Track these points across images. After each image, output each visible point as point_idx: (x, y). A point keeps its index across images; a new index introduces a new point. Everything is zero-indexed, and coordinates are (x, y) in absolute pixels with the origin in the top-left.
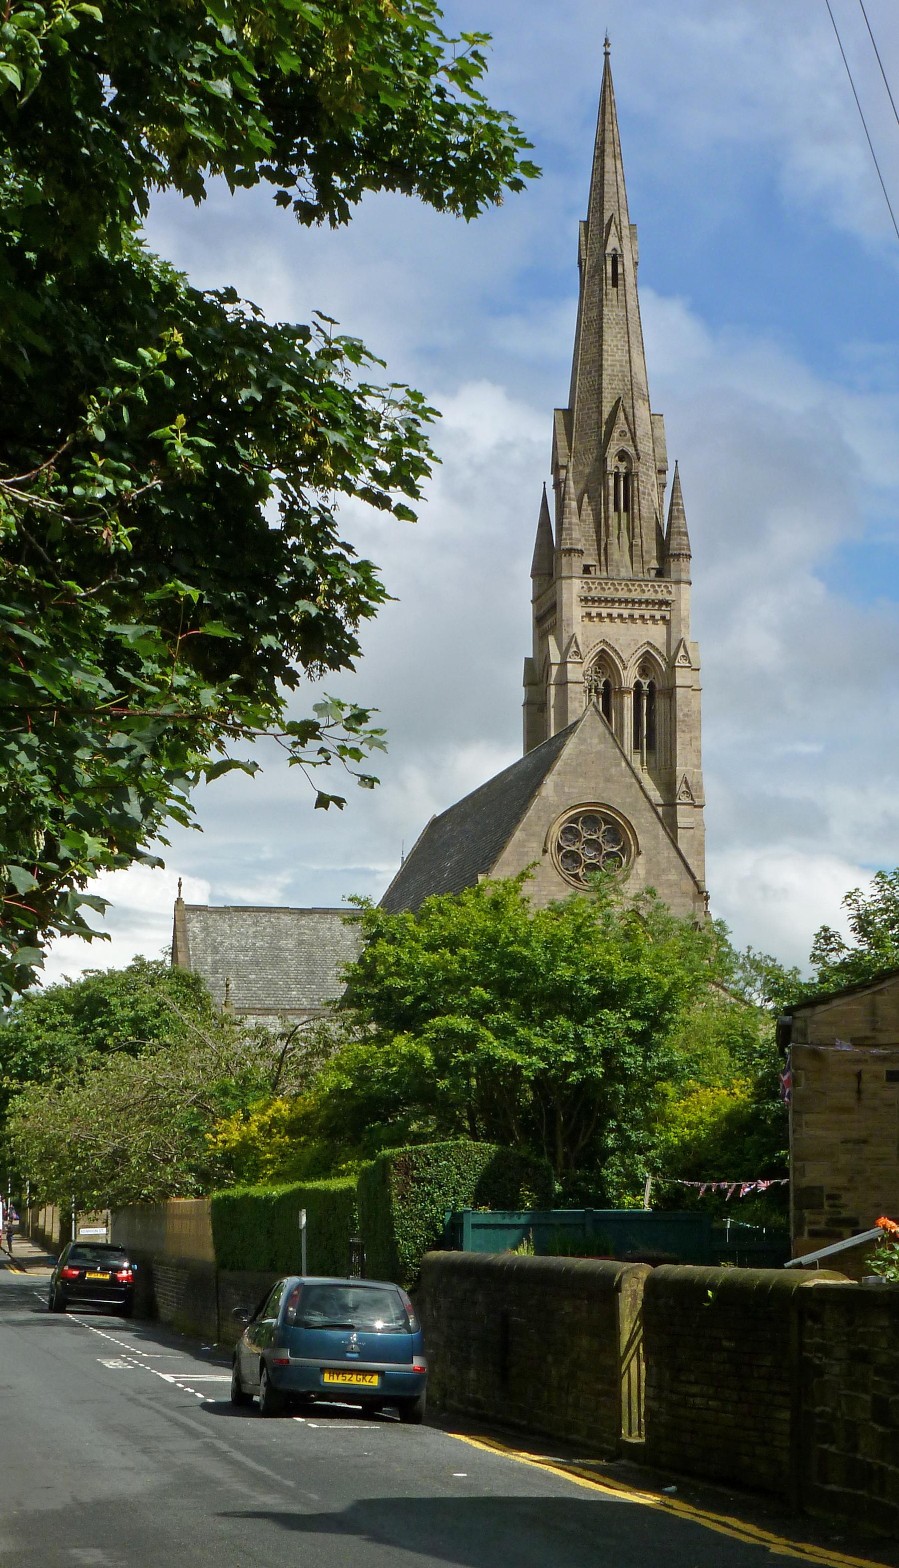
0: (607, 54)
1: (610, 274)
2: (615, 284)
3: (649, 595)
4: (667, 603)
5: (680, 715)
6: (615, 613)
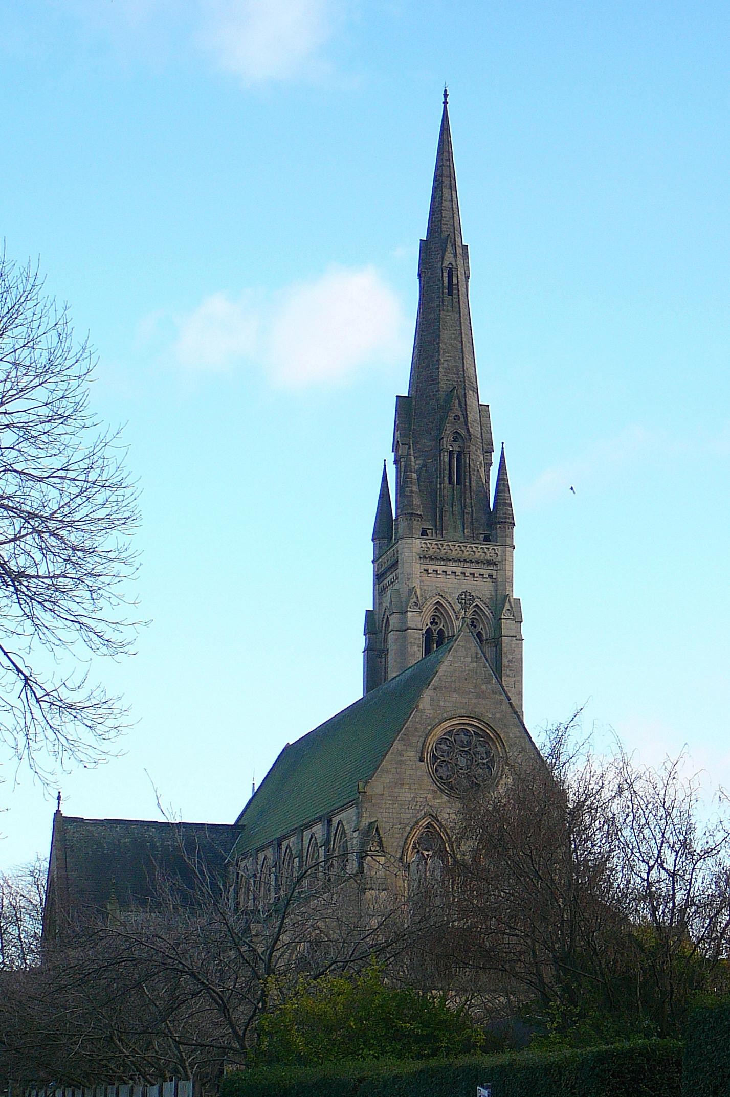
0: (445, 103)
1: (446, 284)
2: (450, 293)
4: (490, 563)
5: (505, 661)
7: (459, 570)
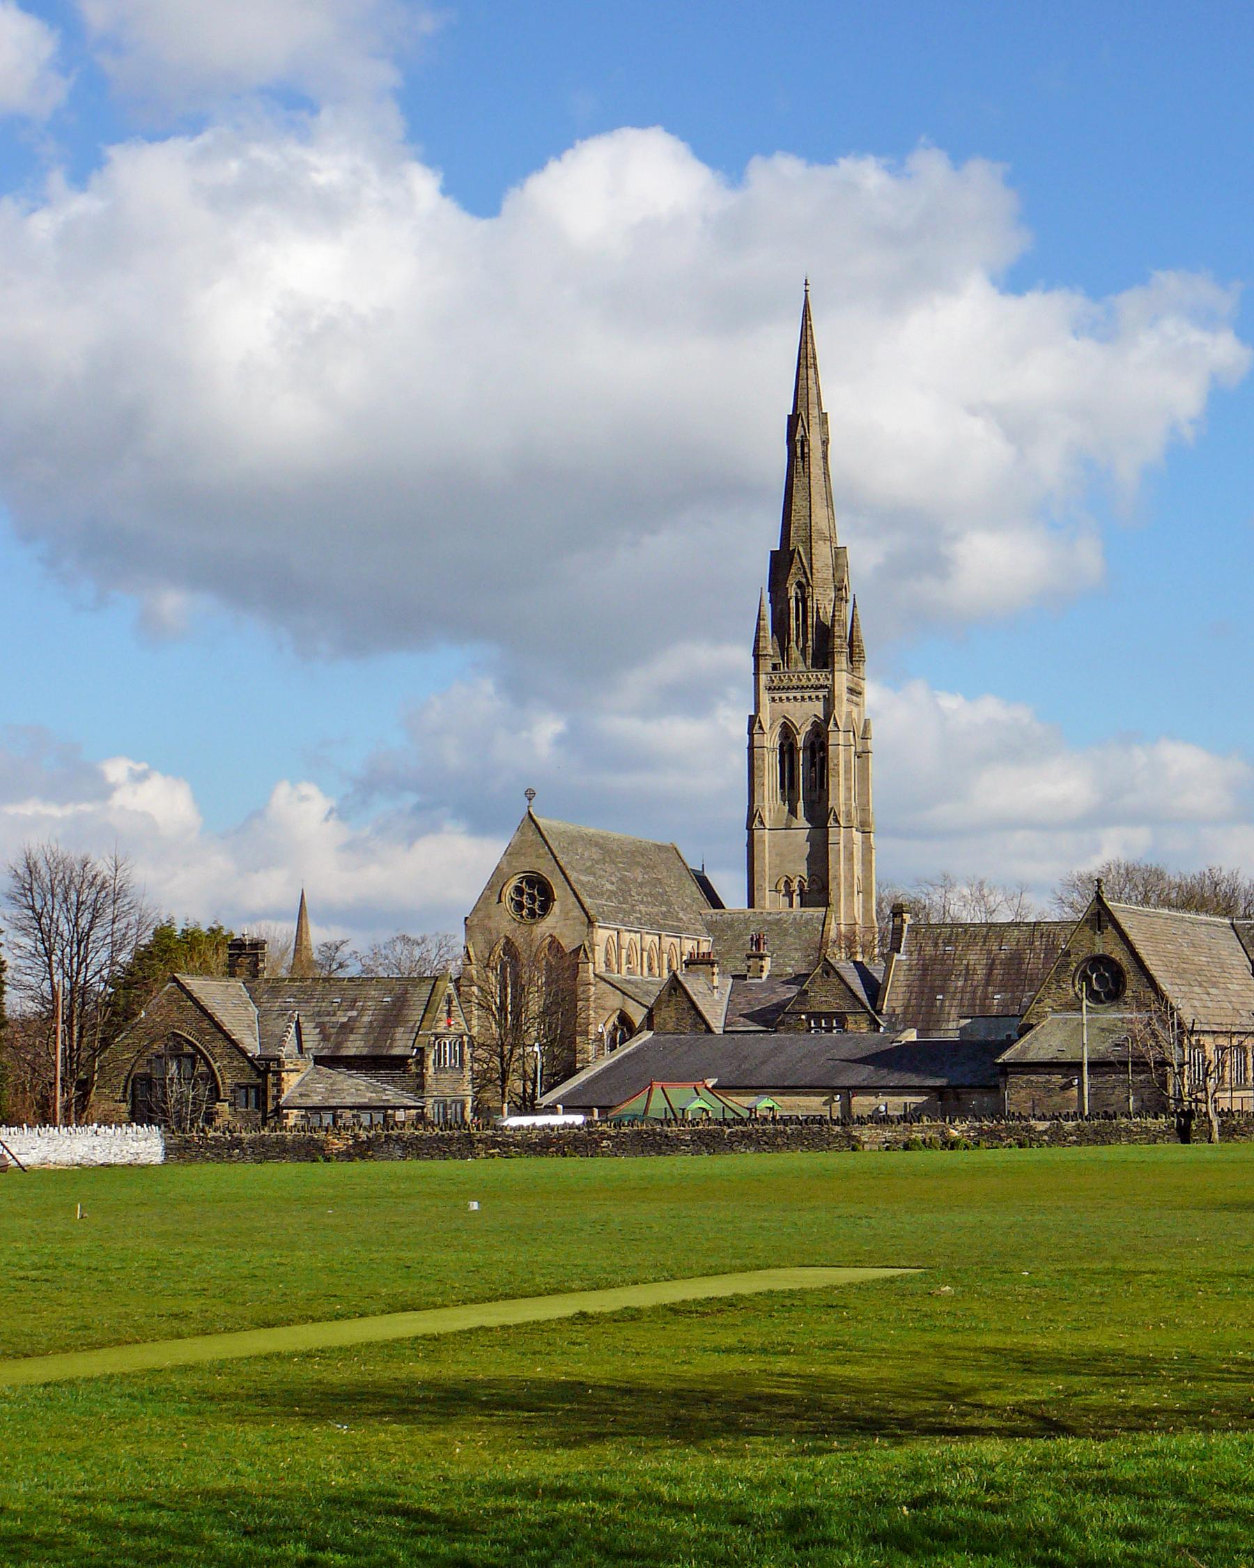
2: (803, 458)
3: (813, 681)
6: (791, 696)
7: (799, 695)
